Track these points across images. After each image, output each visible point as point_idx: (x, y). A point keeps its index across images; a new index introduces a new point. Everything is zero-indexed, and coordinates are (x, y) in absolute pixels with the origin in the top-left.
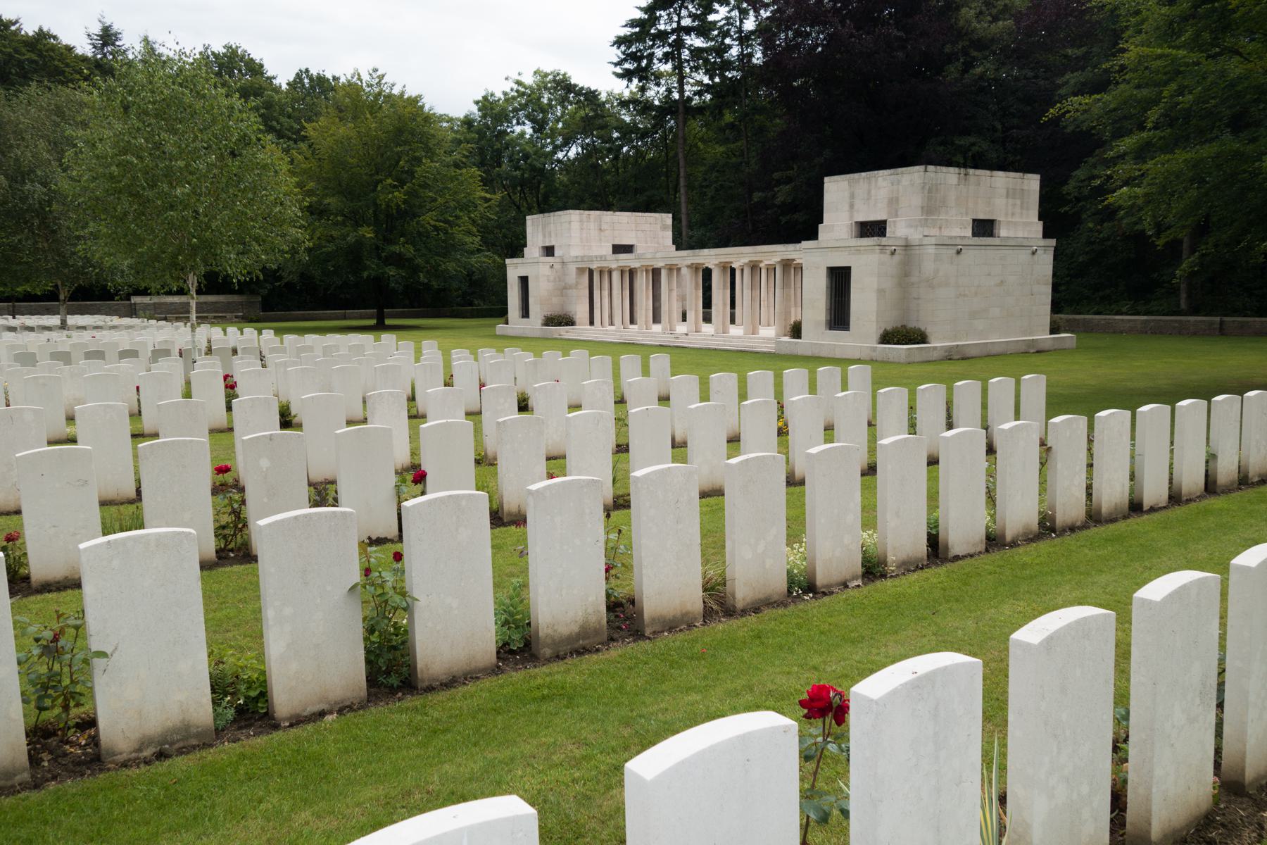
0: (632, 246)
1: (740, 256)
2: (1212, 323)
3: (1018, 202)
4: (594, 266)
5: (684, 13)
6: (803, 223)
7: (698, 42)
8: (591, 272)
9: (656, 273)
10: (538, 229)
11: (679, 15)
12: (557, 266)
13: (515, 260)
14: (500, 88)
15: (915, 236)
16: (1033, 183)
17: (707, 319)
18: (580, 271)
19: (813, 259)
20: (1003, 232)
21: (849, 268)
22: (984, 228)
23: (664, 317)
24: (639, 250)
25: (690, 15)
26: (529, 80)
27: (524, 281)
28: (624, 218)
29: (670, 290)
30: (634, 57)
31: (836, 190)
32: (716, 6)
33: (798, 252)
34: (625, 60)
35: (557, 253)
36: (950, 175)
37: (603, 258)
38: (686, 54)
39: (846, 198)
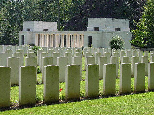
0: (48, 29)
1: (72, 33)
3: (125, 25)
4: (40, 34)
6: (84, 27)
8: (39, 35)
9: (54, 35)
10: (26, 25)
15: (104, 30)
16: (128, 21)
20: (121, 30)
22: (118, 29)
24: (50, 30)
27: (23, 37)
28: (47, 23)
29: (57, 39)
31: (90, 21)
32: (59, 101)
33: (78, 33)
36: (110, 20)
39: (92, 22)
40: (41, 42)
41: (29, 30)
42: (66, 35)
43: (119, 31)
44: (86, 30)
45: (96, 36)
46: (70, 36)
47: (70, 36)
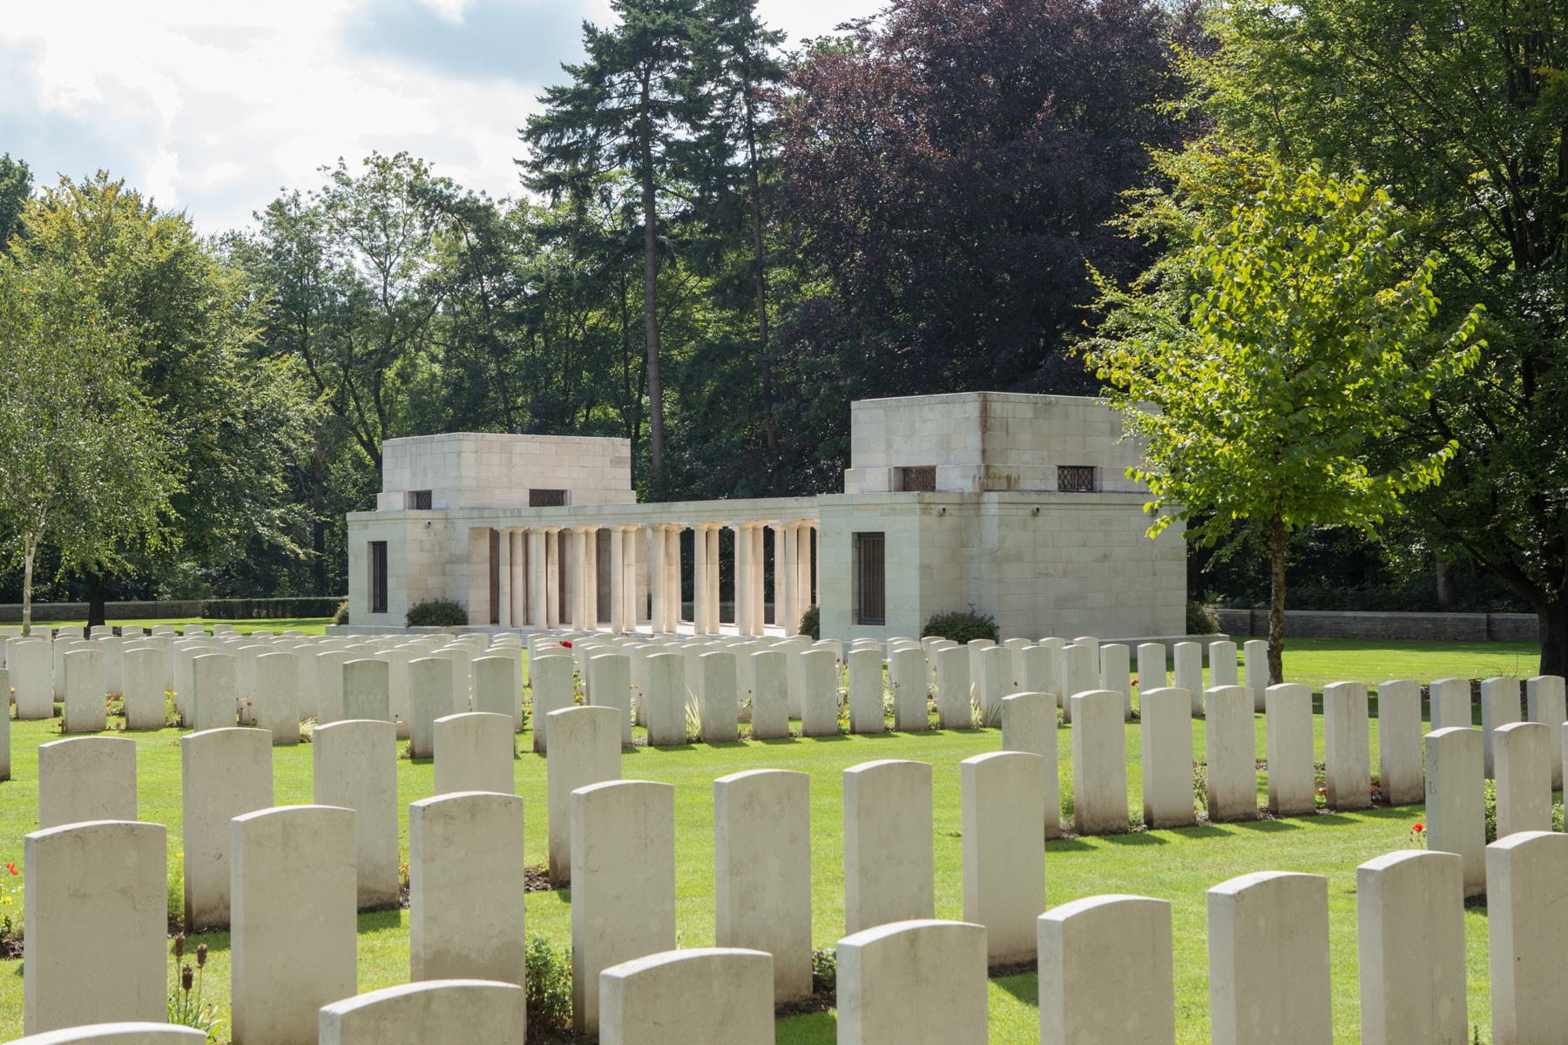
0: (562, 492)
2: (1477, 622)
4: (503, 526)
5: (655, 78)
7: (682, 133)
8: (495, 536)
9: (603, 537)
11: (645, 82)
12: (438, 526)
13: (364, 515)
14: (307, 184)
17: (688, 615)
18: (476, 532)
19: (829, 518)
21: (882, 535)
23: (617, 610)
24: (574, 499)
25: (667, 84)
26: (358, 171)
27: (379, 549)
30: (568, 154)
31: (867, 416)
33: (788, 514)
34: (549, 160)
35: (436, 502)
37: (516, 513)
38: (658, 149)
39: (893, 432)
40: (783, 580)
41: (422, 500)
42: (736, 529)
43: (1091, 490)
44: (839, 487)
45: (908, 534)
46: (769, 534)
47: (769, 534)
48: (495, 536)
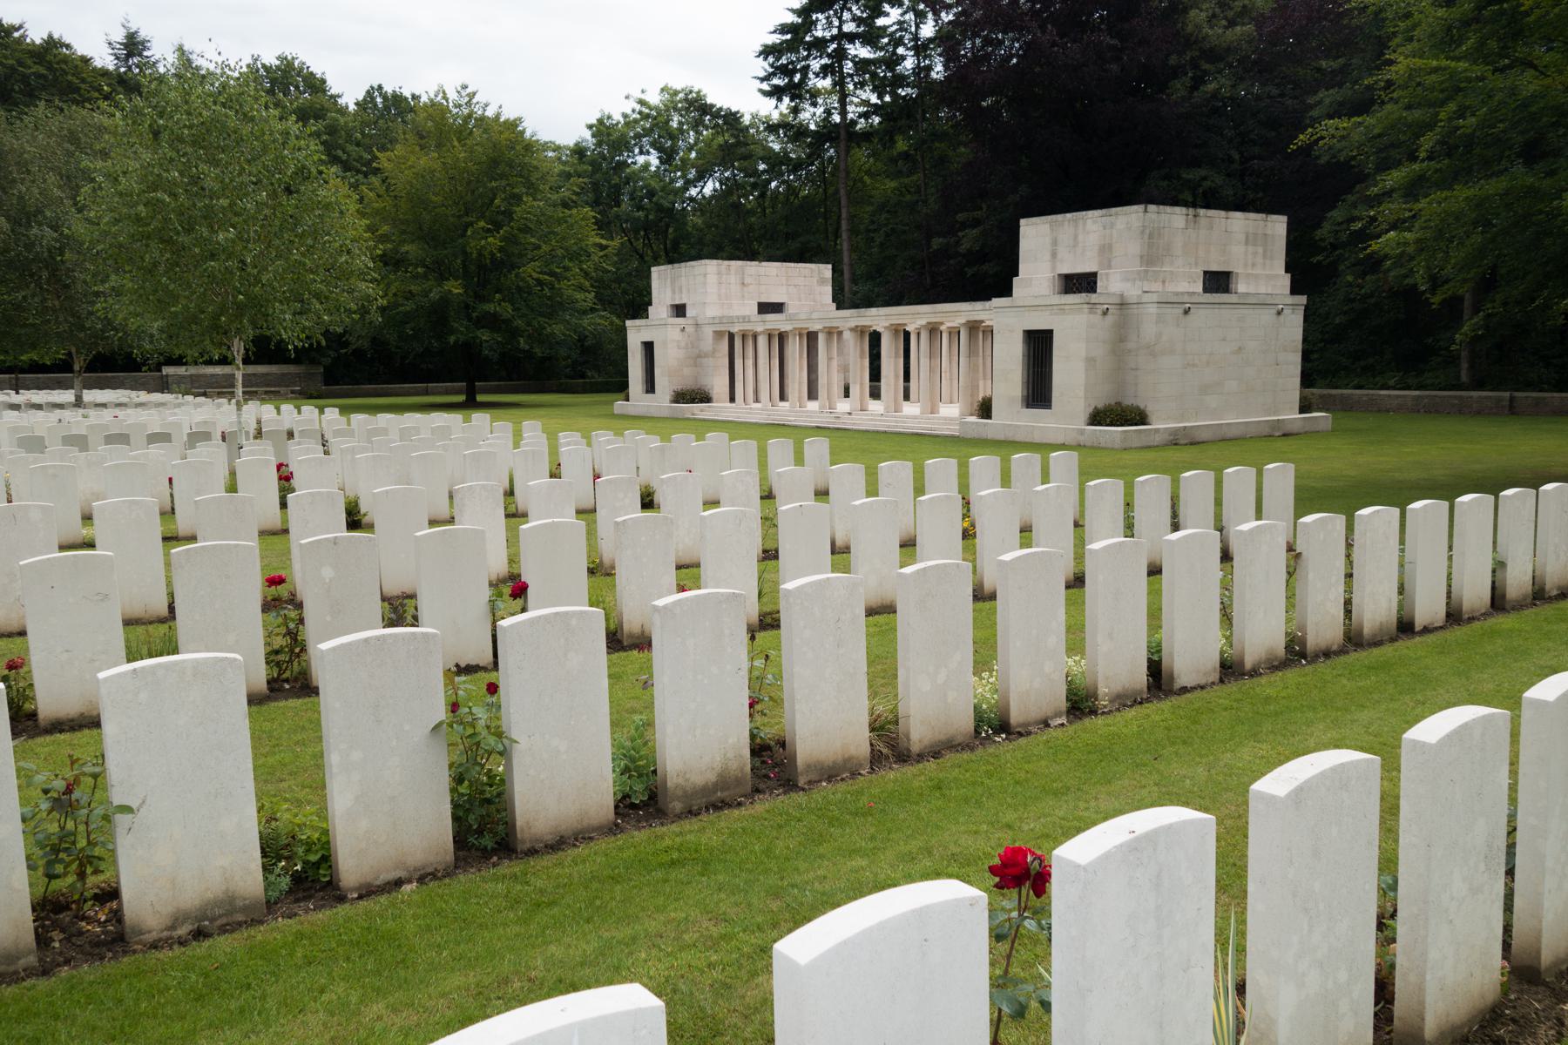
0: (782, 305)
1: (916, 316)
2: (1499, 400)
3: (1260, 250)
4: (735, 330)
5: (846, 16)
6: (994, 275)
7: (864, 52)
8: (731, 337)
9: (812, 337)
10: (665, 283)
11: (840, 18)
12: (690, 329)
13: (637, 322)
14: (619, 109)
15: (1132, 291)
16: (1278, 226)
17: (875, 394)
18: (718, 335)
19: (1006, 320)
20: (1241, 287)
21: (1051, 332)
22: (1218, 282)
23: (822, 392)
24: (791, 309)
25: (854, 19)
26: (655, 99)
27: (649, 347)
28: (773, 269)
29: (830, 359)
30: (785, 71)
31: (1035, 234)
32: (887, 7)
33: (988, 311)
34: (773, 74)
35: (689, 313)
36: (1175, 217)
37: (746, 319)
38: (848, 67)
39: (1046, 245)
48: (907, 335)
